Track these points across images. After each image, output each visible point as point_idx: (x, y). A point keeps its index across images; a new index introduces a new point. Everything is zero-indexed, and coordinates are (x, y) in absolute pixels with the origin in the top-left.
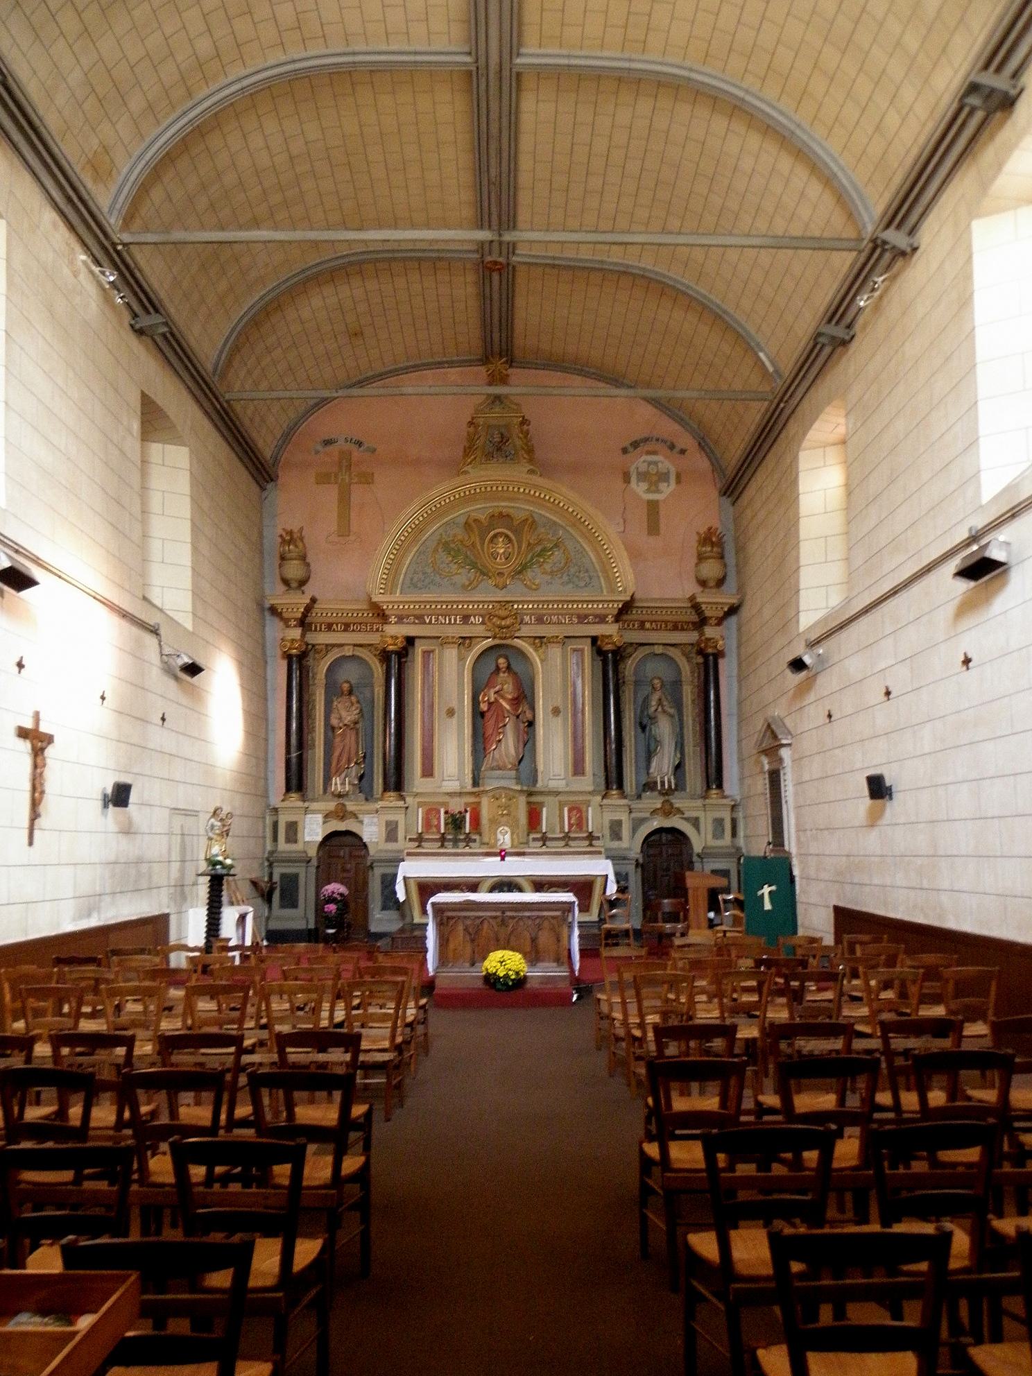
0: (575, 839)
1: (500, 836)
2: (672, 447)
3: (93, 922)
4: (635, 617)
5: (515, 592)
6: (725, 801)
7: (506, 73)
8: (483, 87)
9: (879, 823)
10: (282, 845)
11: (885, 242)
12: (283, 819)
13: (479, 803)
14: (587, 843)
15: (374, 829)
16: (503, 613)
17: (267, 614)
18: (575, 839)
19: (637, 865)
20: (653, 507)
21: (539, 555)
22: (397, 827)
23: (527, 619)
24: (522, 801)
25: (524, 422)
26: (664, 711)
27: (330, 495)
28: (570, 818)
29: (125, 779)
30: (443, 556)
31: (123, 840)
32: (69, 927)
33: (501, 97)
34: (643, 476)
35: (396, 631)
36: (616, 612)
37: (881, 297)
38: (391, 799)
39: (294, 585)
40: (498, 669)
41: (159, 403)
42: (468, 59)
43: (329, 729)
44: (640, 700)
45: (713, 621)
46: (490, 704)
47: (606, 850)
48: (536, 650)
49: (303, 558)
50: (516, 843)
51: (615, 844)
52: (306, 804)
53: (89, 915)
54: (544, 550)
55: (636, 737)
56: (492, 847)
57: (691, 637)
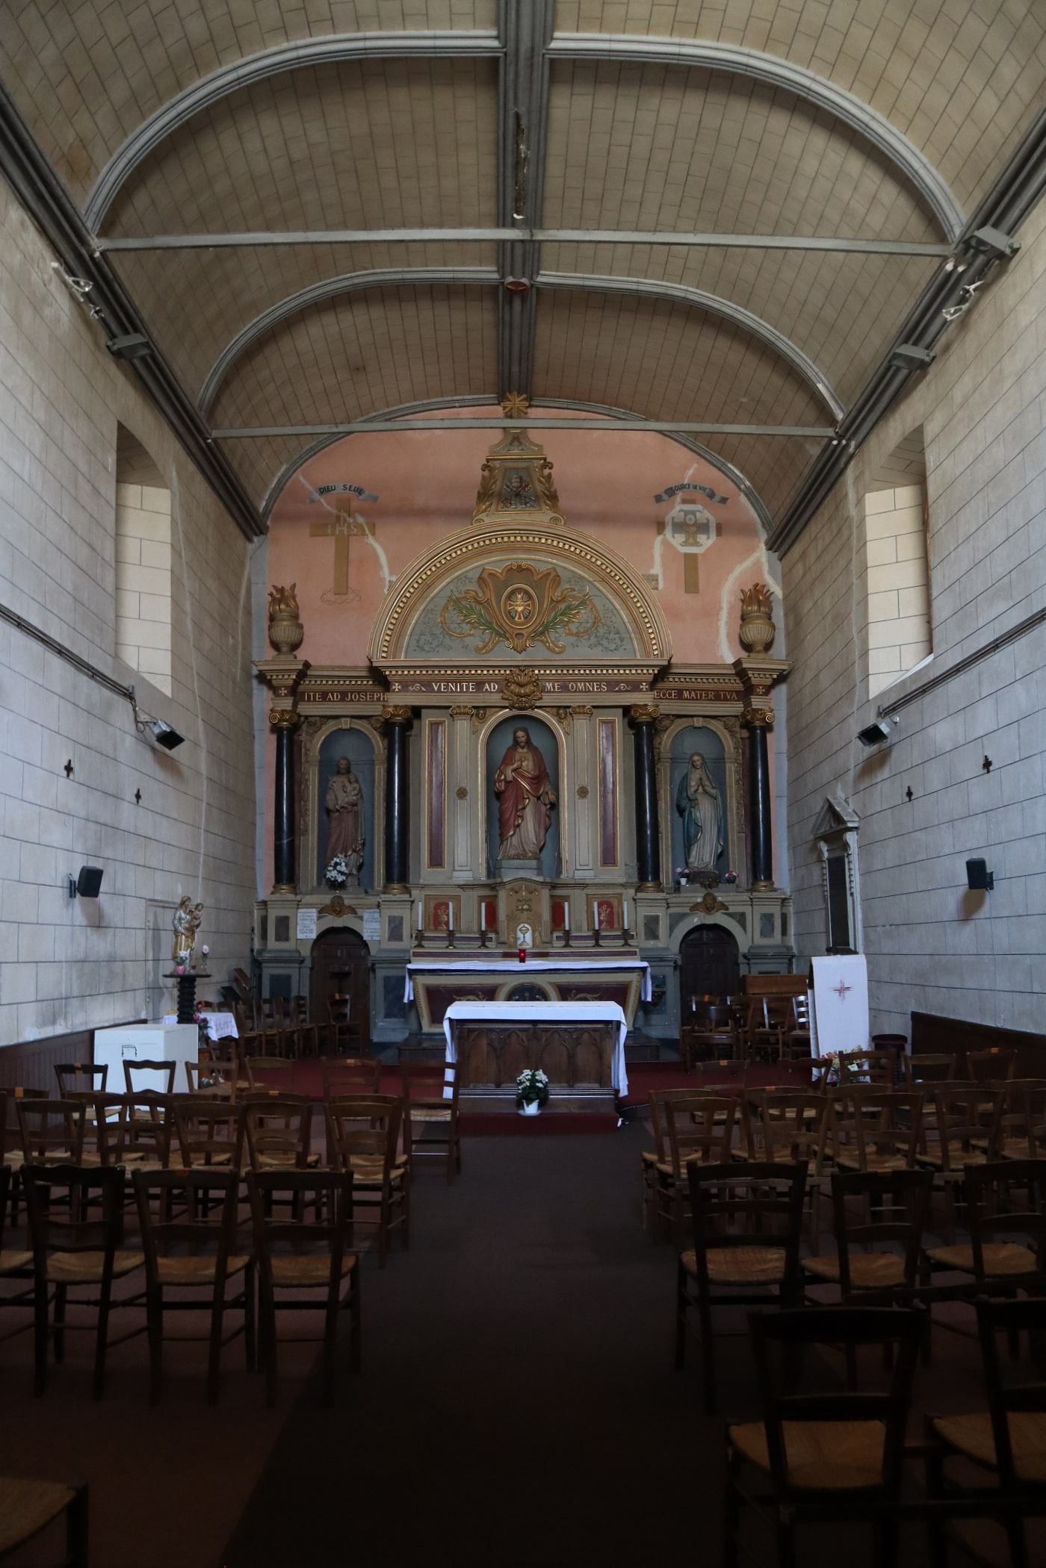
0: (606, 937)
1: (520, 935)
2: (711, 495)
3: (60, 1029)
4: (672, 685)
5: (536, 654)
6: (773, 895)
7: (538, 59)
8: (511, 77)
9: (975, 916)
10: (272, 944)
11: (981, 242)
12: (273, 915)
13: (496, 896)
14: (622, 942)
15: (377, 926)
16: (522, 679)
17: (255, 682)
18: (606, 937)
19: (675, 968)
20: (691, 561)
23: (549, 686)
24: (545, 893)
25: (547, 465)
26: (706, 792)
27: (325, 549)
28: (599, 914)
29: (96, 864)
30: (454, 616)
31: (93, 936)
32: (31, 1033)
33: (531, 89)
34: (679, 527)
35: (399, 698)
36: (650, 678)
37: (969, 311)
38: (396, 893)
39: (285, 649)
40: (516, 742)
42: (495, 43)
43: (326, 811)
44: (678, 779)
45: (761, 690)
46: (508, 783)
47: (641, 950)
48: (560, 722)
49: (295, 616)
50: (538, 941)
51: (651, 944)
52: (298, 897)
53: (54, 1023)
54: (569, 608)
55: (672, 820)
56: (511, 947)
57: (736, 708)
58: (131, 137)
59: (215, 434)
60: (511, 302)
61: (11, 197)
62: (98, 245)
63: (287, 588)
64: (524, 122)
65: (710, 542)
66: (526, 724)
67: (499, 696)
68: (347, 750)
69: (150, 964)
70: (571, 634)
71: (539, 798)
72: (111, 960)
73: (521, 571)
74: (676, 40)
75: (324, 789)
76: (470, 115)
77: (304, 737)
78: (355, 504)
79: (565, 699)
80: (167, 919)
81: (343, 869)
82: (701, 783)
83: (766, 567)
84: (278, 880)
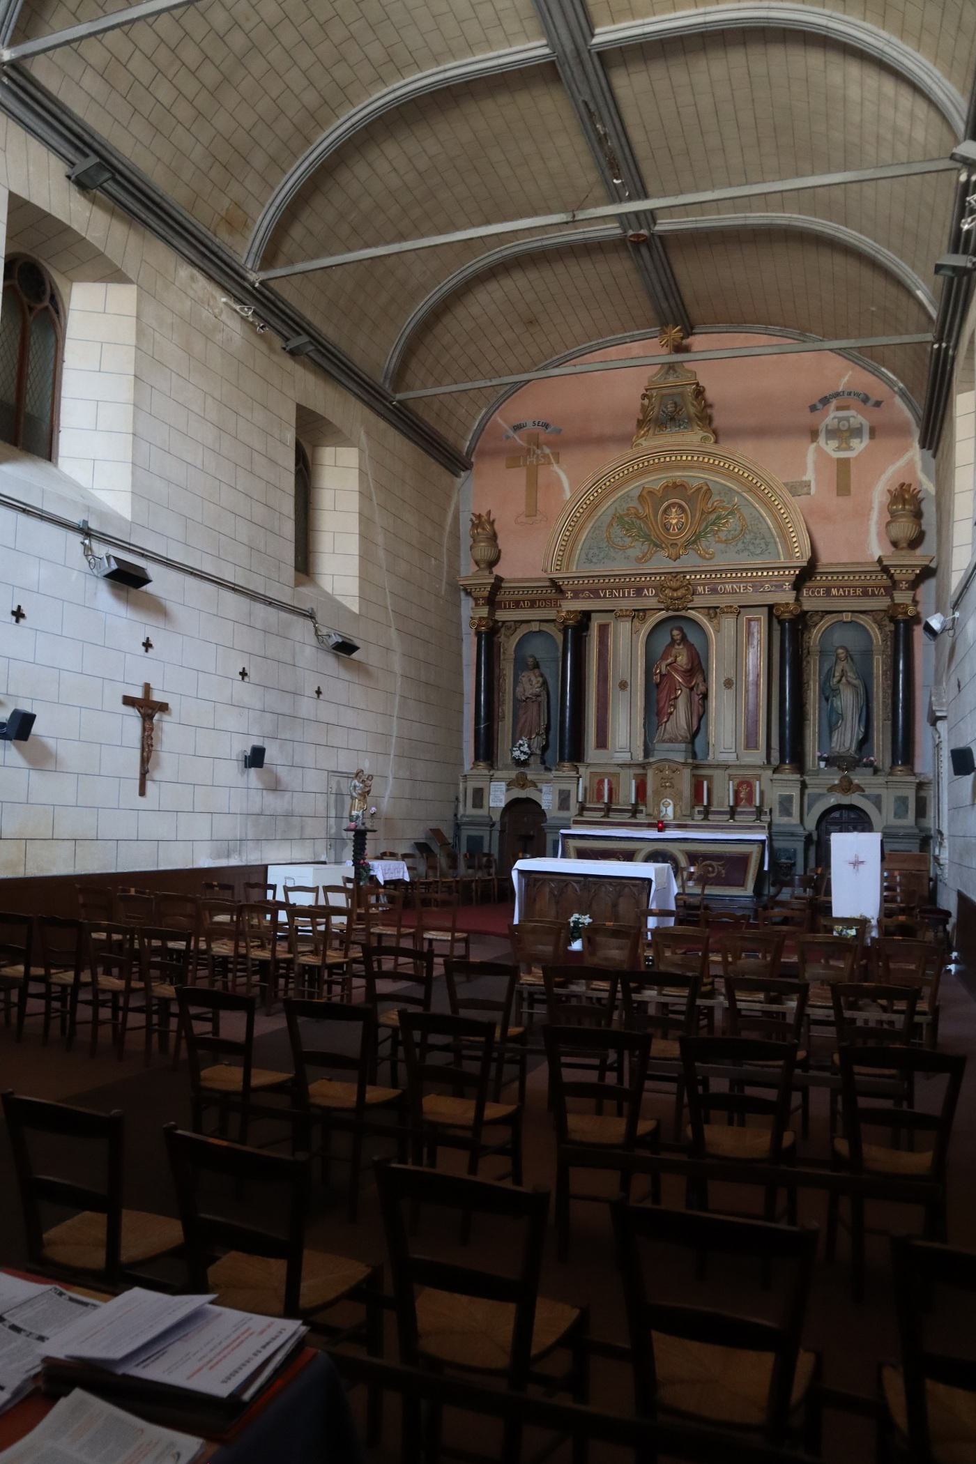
0: (742, 813)
2: (866, 400)
3: (234, 862)
4: (820, 584)
5: (689, 561)
7: (585, 56)
10: (471, 811)
15: (550, 797)
16: (674, 584)
17: (462, 594)
18: (742, 813)
20: (843, 465)
21: (714, 524)
22: (569, 796)
23: (700, 589)
24: (687, 773)
27: (518, 478)
30: (617, 531)
32: (204, 862)
34: (832, 433)
35: (573, 605)
38: (567, 770)
40: (673, 641)
41: (320, 411)
45: (904, 585)
46: (662, 676)
50: (678, 815)
53: (228, 856)
54: (719, 518)
57: (882, 603)
58: (277, 190)
59: (399, 396)
60: (639, 251)
61: (180, 260)
62: (255, 277)
63: (484, 514)
64: (592, 106)
65: (863, 446)
66: (682, 624)
67: (655, 600)
68: (537, 649)
69: (332, 821)
70: (720, 541)
71: (692, 689)
72: (289, 815)
73: (677, 488)
74: (702, 10)
75: (516, 682)
76: (550, 107)
77: (502, 639)
78: (542, 438)
79: (713, 601)
80: (346, 785)
81: (525, 749)
82: (843, 674)
83: (919, 465)
84: (477, 758)
